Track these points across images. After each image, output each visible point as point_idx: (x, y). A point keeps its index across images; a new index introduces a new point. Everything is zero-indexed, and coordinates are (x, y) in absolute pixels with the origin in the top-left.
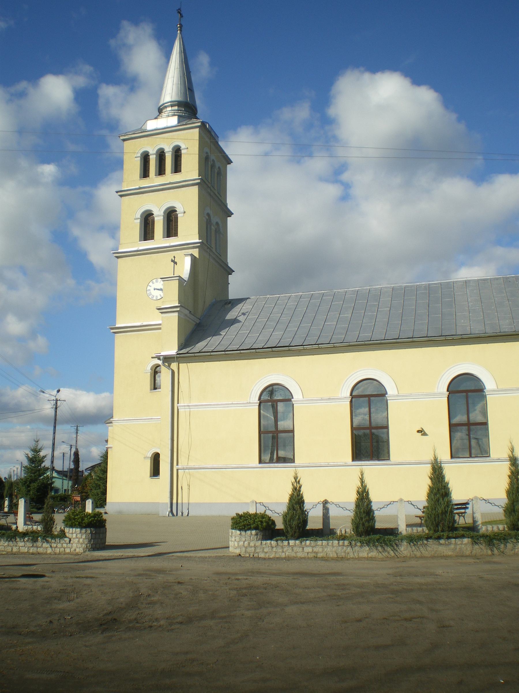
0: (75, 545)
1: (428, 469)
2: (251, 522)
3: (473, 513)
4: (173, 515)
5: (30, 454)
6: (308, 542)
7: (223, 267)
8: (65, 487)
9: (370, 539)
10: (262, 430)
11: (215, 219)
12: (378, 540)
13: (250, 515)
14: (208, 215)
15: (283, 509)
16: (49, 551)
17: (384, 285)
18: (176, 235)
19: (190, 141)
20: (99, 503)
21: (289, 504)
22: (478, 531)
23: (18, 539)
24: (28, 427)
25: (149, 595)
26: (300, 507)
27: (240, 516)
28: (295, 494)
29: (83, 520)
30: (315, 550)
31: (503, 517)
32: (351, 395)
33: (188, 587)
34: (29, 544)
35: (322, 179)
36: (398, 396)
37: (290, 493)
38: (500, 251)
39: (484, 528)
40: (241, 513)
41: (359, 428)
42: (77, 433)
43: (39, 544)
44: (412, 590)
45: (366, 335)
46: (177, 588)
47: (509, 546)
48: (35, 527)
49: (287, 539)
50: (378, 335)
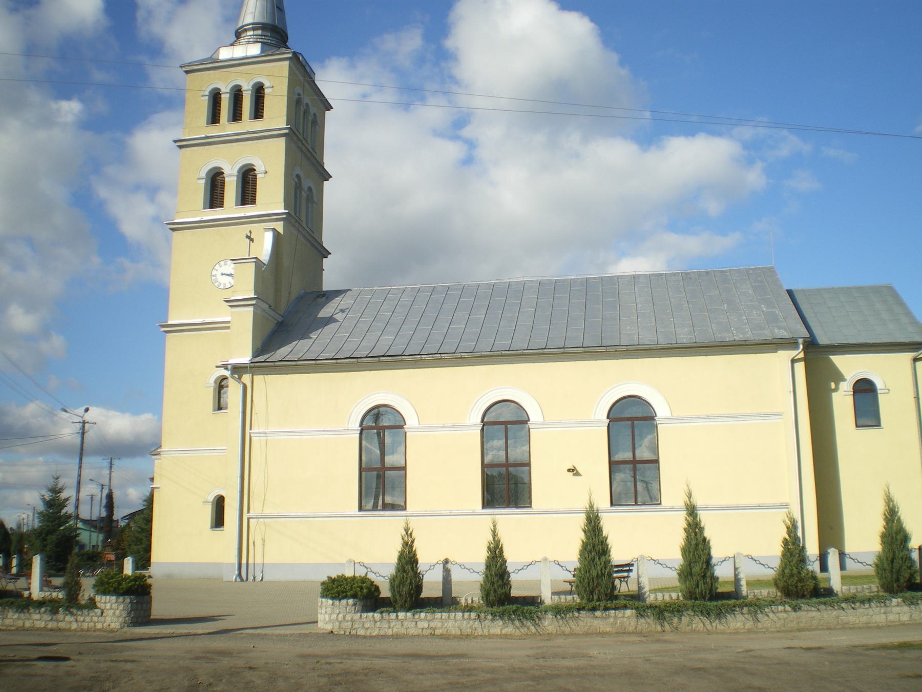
0: (109, 619)
1: (582, 519)
2: (348, 588)
3: (639, 577)
4: (242, 580)
5: (48, 496)
6: (423, 615)
7: (316, 248)
8: (94, 543)
9: (505, 611)
10: (363, 466)
11: (306, 184)
12: (514, 612)
13: (346, 579)
14: (298, 176)
15: (391, 571)
16: (74, 626)
17: (519, 277)
18: (253, 202)
19: (276, 78)
20: (140, 564)
21: (398, 564)
22: (644, 600)
23: (32, 610)
24: (41, 459)
25: (210, 684)
26: (413, 568)
27: (332, 581)
28: (406, 551)
29: (120, 584)
30: (433, 625)
31: (677, 584)
32: (482, 421)
33: (262, 673)
34: (47, 617)
35: (438, 133)
36: (544, 424)
37: (400, 549)
38: (672, 238)
39: (652, 597)
40: (334, 576)
41: (492, 465)
42: (111, 467)
43: (60, 616)
44: (558, 676)
45: (503, 343)
46: (249, 675)
47: (685, 620)
48: (54, 594)
49: (395, 611)
50: (520, 343)
